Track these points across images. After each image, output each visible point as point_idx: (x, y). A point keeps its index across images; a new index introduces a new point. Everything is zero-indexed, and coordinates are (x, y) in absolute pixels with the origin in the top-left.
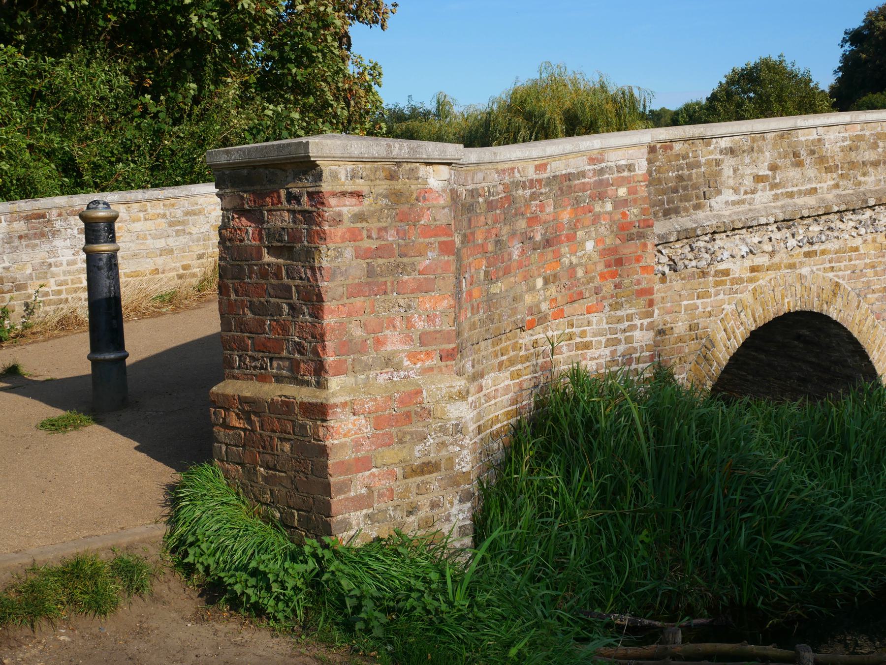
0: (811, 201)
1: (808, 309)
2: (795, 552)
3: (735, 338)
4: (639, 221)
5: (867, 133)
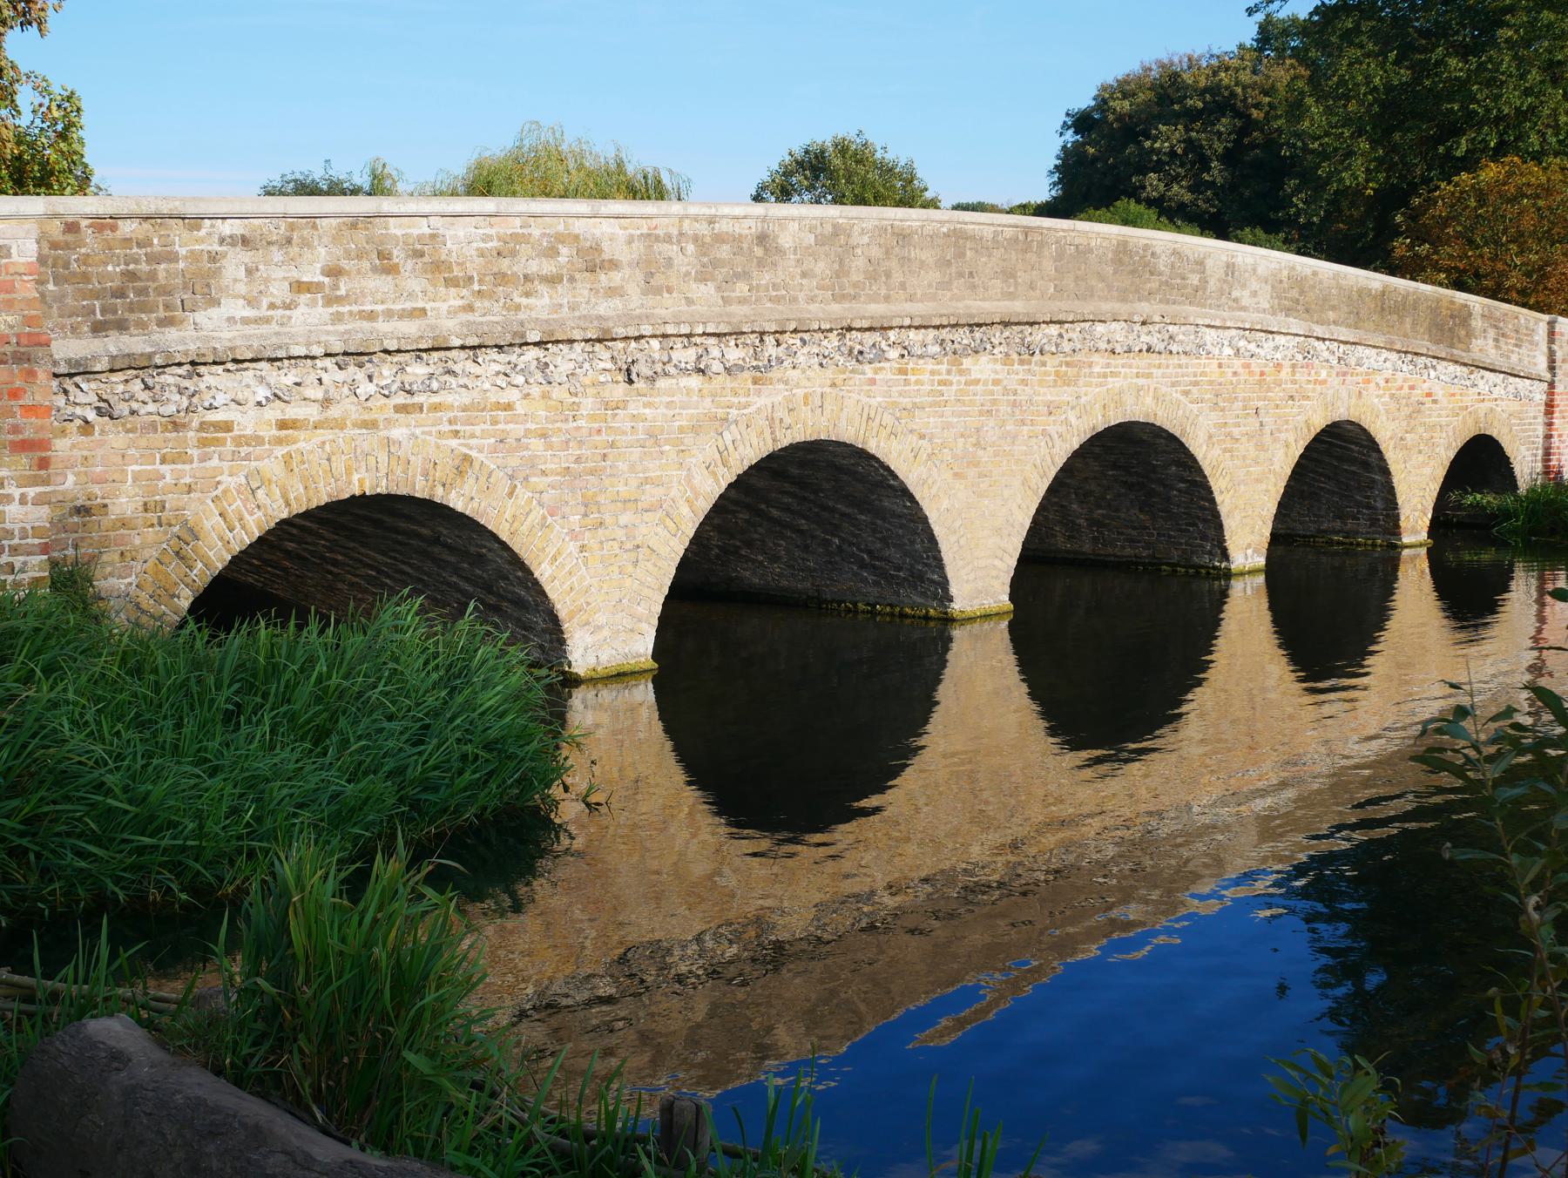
0: (410, 328)
1: (403, 491)
2: (22, 835)
3: (243, 527)
4: (18, 335)
5: (536, 232)
